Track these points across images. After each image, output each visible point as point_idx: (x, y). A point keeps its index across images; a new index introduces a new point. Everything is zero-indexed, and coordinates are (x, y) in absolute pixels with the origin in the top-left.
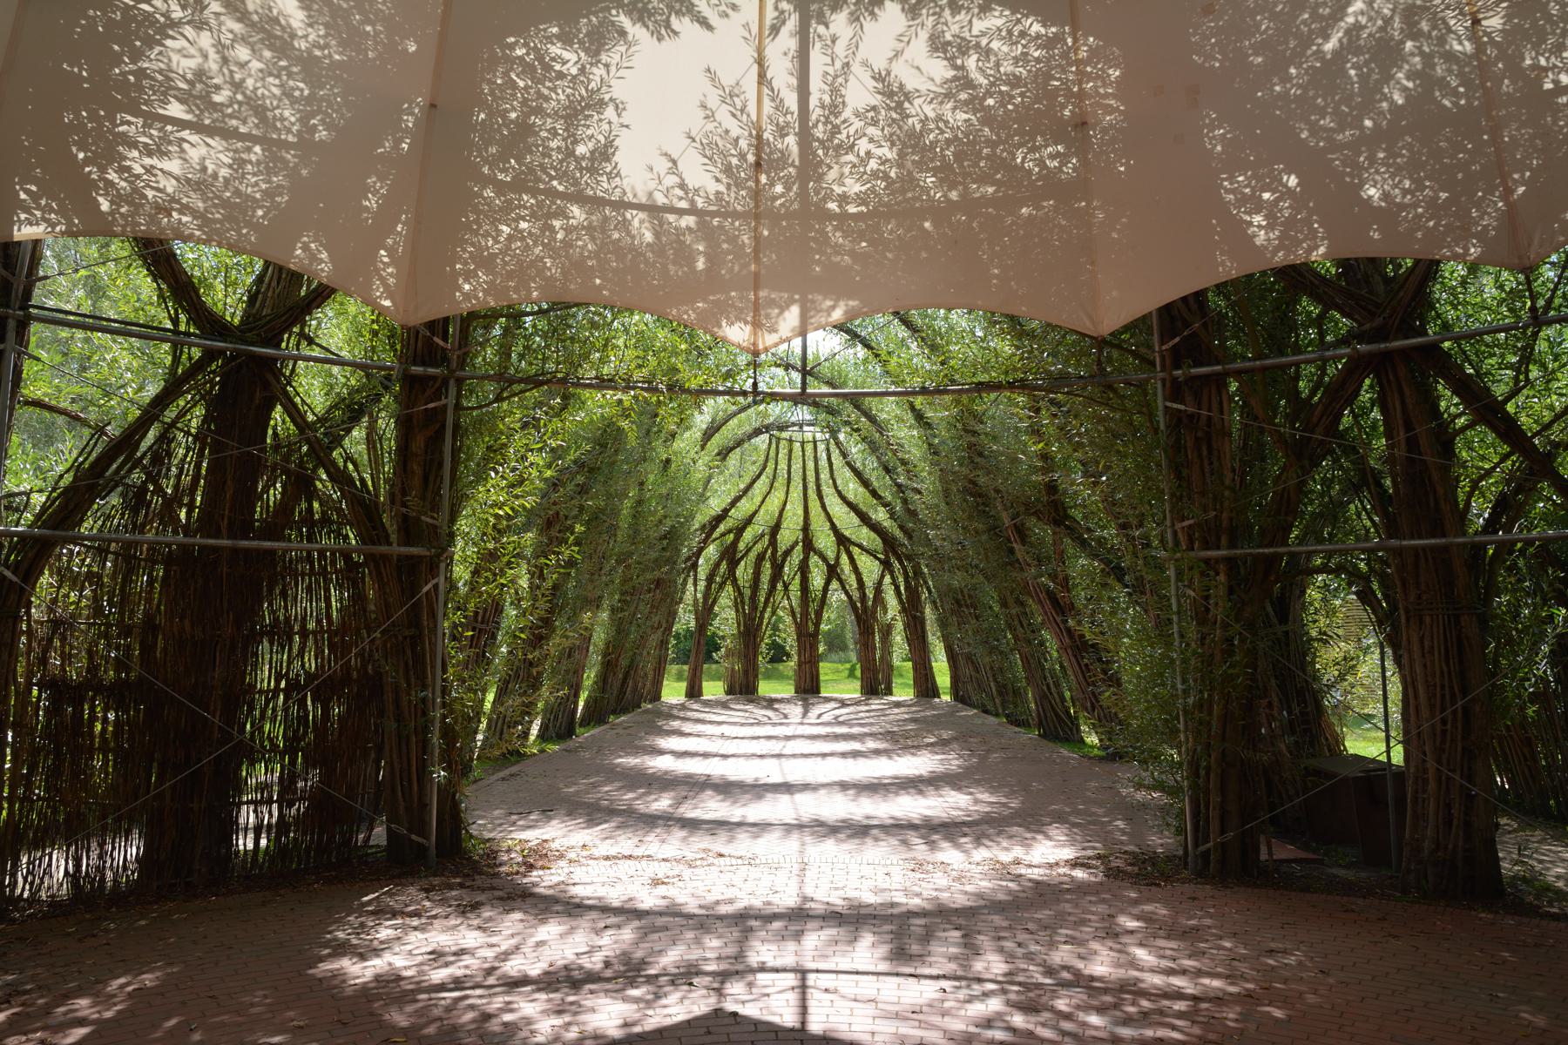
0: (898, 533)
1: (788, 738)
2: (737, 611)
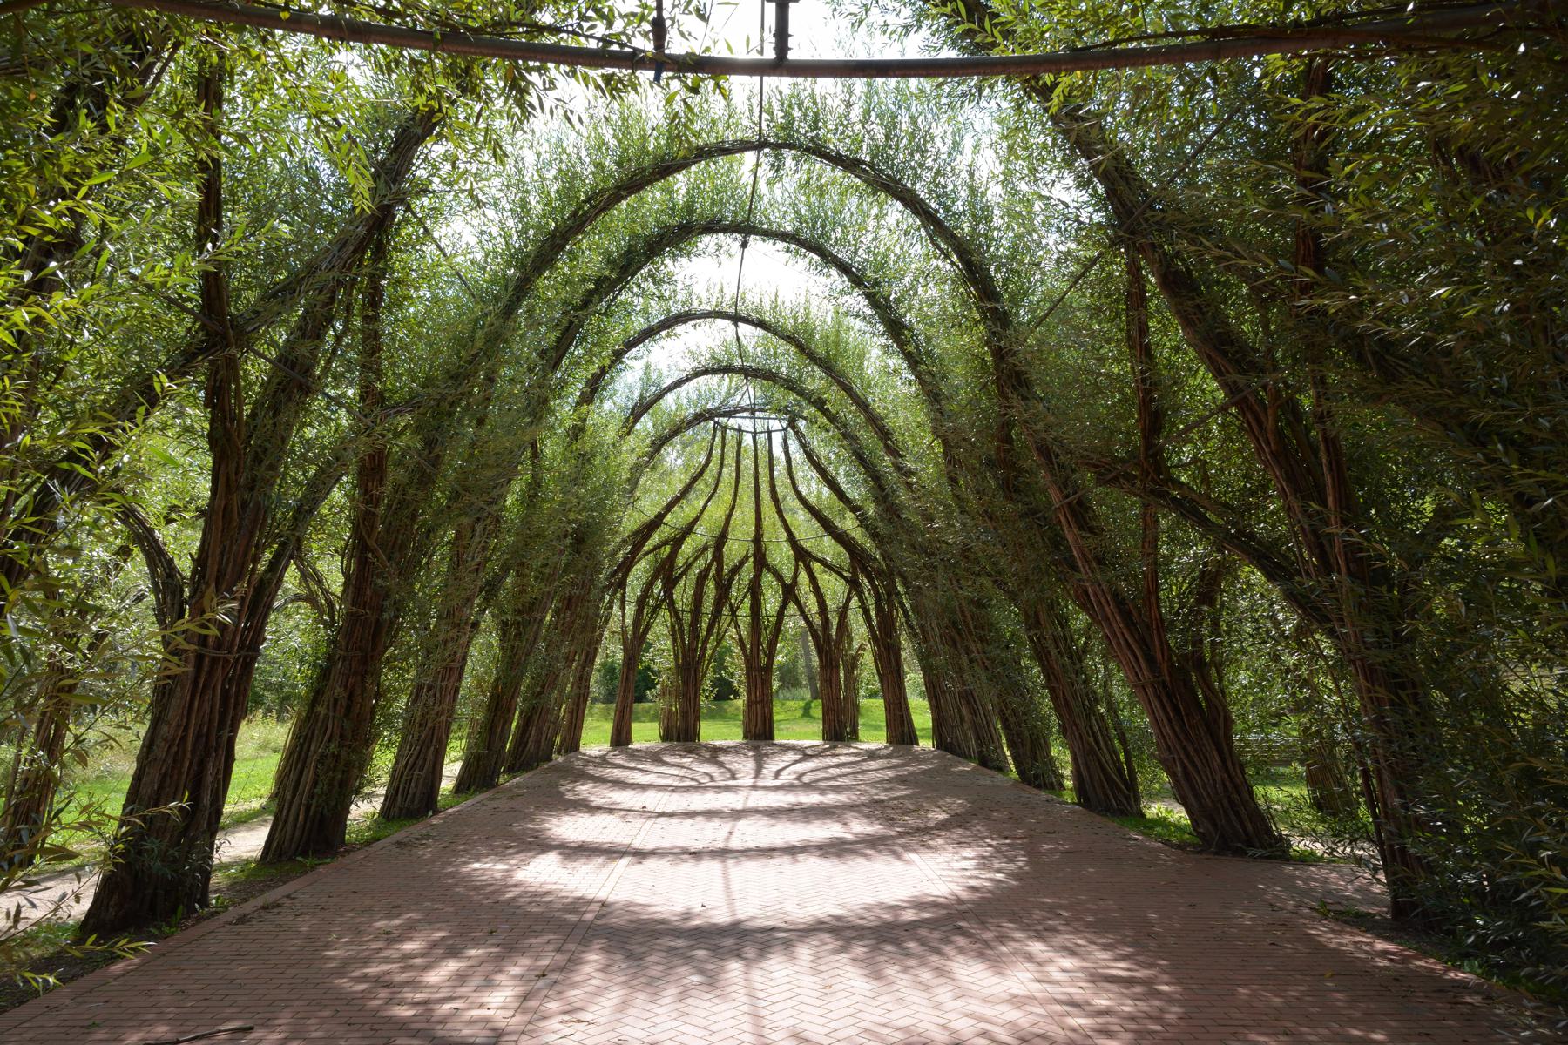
0: (869, 544)
1: (738, 814)
2: (675, 641)
